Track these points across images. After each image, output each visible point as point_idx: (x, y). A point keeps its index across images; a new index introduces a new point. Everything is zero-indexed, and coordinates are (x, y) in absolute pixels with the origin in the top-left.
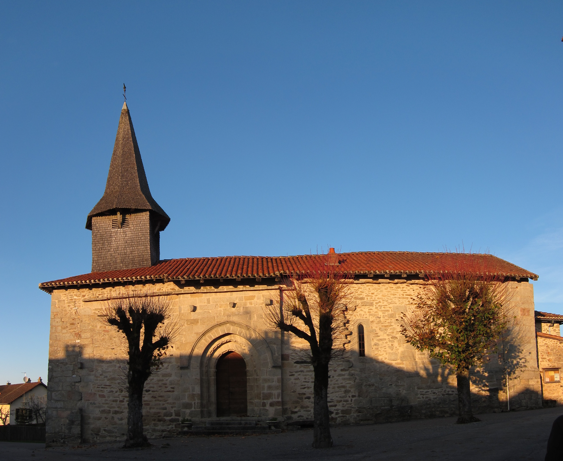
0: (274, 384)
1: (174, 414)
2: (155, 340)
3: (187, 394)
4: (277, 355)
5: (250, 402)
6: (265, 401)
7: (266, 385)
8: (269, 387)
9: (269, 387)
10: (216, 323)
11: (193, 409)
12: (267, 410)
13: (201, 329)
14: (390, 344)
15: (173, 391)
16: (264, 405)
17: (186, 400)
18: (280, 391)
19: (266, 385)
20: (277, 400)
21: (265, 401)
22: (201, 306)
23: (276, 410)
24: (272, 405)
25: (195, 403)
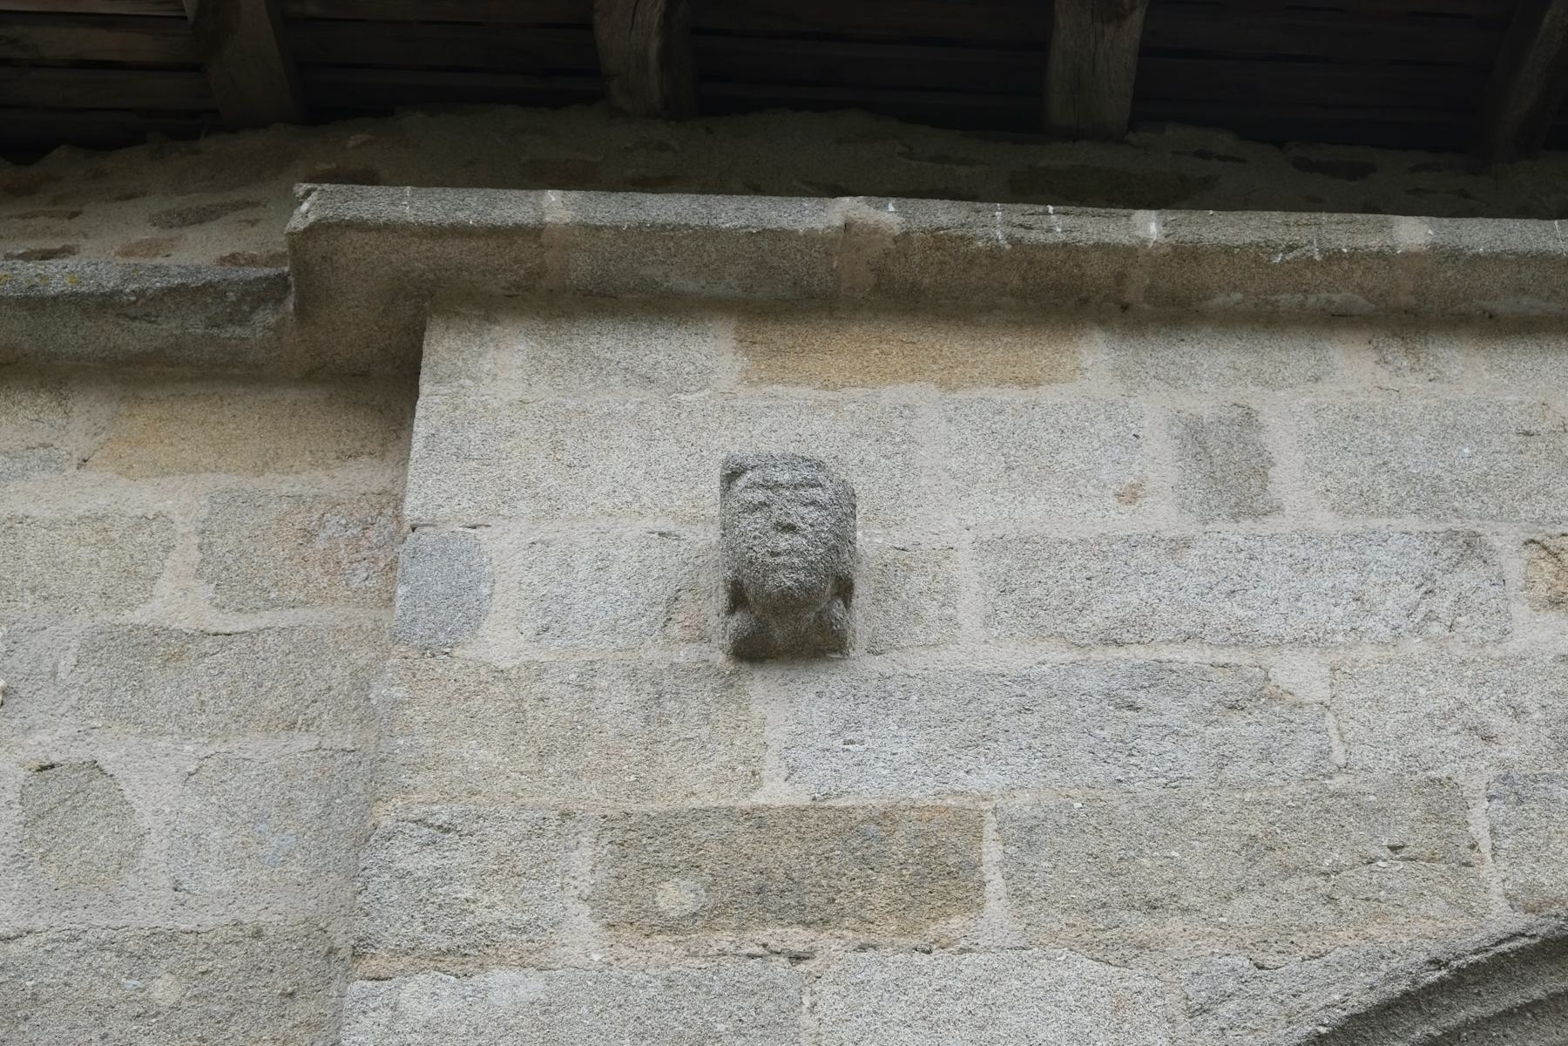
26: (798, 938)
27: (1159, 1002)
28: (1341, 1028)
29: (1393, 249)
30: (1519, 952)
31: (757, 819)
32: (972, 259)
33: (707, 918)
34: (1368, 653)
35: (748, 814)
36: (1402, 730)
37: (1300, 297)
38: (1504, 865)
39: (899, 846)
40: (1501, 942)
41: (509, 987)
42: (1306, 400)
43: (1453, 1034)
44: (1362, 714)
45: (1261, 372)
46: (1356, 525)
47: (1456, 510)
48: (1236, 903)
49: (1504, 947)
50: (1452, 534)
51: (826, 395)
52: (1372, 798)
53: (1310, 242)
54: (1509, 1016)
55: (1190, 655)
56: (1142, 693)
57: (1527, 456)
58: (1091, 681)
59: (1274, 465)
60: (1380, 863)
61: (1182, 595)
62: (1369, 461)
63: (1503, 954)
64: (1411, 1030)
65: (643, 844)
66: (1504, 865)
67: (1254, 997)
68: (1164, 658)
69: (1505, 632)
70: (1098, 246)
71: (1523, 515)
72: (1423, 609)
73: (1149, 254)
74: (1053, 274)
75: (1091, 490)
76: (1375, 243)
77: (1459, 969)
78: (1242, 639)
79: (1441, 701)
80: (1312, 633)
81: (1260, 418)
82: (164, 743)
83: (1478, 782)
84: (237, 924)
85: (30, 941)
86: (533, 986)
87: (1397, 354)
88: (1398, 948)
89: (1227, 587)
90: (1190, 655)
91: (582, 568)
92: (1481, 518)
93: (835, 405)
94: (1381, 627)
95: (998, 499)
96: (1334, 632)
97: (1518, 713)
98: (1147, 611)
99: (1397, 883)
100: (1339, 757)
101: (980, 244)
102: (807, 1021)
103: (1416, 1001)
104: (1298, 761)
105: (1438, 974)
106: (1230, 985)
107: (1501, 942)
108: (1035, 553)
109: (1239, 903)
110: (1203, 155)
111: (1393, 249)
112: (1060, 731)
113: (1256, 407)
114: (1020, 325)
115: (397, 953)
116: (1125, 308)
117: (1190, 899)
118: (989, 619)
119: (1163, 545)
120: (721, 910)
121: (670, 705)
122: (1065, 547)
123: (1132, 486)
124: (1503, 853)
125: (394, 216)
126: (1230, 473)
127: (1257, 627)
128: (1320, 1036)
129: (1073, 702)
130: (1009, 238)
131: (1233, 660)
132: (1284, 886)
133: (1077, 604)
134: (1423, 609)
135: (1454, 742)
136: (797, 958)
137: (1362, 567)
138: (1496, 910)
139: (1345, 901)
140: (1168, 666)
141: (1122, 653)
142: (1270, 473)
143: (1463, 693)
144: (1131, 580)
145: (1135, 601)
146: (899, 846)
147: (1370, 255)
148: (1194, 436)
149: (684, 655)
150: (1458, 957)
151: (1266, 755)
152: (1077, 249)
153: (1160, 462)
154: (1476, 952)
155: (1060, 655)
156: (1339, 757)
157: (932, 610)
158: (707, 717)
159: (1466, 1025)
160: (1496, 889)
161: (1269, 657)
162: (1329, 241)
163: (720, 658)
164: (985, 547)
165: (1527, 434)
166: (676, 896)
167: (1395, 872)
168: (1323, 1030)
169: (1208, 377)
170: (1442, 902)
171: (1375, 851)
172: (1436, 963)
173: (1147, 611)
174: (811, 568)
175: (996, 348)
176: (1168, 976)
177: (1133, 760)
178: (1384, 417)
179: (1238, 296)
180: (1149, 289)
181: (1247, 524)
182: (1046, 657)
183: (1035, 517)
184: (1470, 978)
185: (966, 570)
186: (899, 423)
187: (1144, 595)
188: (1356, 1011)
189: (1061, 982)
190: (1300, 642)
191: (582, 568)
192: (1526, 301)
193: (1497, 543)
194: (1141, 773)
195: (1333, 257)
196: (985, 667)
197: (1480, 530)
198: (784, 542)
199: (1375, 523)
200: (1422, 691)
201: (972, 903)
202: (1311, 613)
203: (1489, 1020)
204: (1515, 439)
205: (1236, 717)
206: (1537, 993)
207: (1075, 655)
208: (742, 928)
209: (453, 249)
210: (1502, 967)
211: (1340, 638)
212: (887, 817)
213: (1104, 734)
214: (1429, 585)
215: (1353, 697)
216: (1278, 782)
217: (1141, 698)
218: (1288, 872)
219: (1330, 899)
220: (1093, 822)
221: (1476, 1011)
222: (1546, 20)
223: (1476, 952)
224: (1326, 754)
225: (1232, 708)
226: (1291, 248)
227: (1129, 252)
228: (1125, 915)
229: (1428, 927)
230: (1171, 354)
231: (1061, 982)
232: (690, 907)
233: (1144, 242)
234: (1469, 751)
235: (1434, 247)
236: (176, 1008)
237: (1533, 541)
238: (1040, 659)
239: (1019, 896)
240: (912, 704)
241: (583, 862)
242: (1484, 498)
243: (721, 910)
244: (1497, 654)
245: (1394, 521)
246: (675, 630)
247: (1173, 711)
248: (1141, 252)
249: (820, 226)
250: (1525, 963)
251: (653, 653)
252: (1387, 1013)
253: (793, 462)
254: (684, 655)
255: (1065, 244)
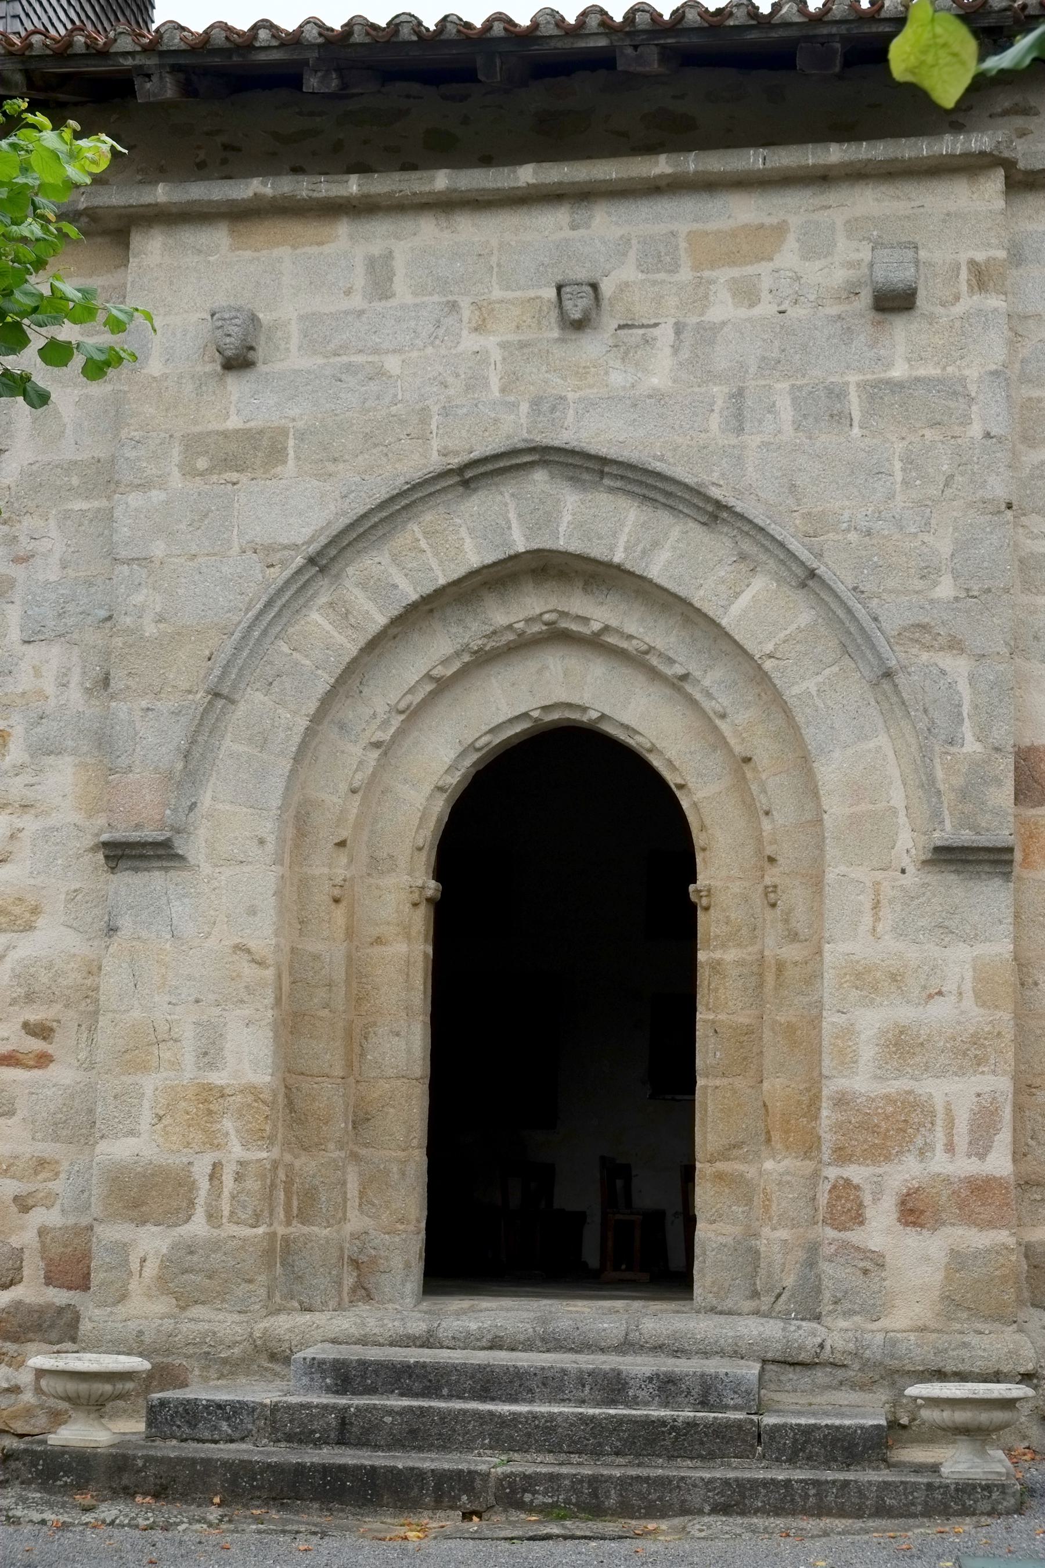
0: (940, 1012)
1: (33, 1268)
2: (754, 22)
3: (149, 1083)
4: (971, 746)
5: (720, 1176)
6: (855, 1173)
7: (871, 1022)
8: (901, 1046)
9: (901, 1046)
10: (435, 462)
11: (198, 1227)
12: (874, 1263)
13: (300, 509)
14: (877, 1377)
15: (43, 1060)
16: (847, 1208)
17: (134, 1146)
18: (1004, 1084)
19: (871, 1022)
20: (966, 1166)
21: (855, 1173)
22: (311, 320)
23: (958, 1260)
24: (913, 1212)
25: (215, 1175)
26: (234, 476)
31: (225, 434)
33: (209, 471)
35: (223, 433)
39: (265, 442)
41: (157, 496)
46: (418, 300)
50: (448, 302)
51: (256, 254)
55: (359, 359)
62: (426, 271)
65: (193, 444)
78: (376, 351)
82: (69, 390)
84: (93, 457)
85: (37, 465)
86: (163, 496)
89: (374, 330)
90: (359, 359)
91: (179, 335)
93: (258, 259)
100: (400, 397)
102: (236, 505)
106: (353, 488)
115: (127, 486)
117: (347, 457)
118: (300, 348)
120: (214, 467)
121: (204, 388)
125: (110, 204)
136: (234, 484)
139: (390, 455)
146: (265, 442)
148: (371, 263)
149: (208, 368)
155: (320, 361)
156: (400, 397)
157: (283, 346)
158: (214, 392)
163: (219, 368)
164: (301, 318)
166: (202, 463)
169: (378, 237)
171: (402, 436)
172: (407, 483)
174: (237, 348)
181: (384, 302)
185: (294, 329)
186: (278, 265)
189: (306, 489)
190: (394, 351)
191: (179, 335)
196: (296, 367)
198: (228, 340)
201: (285, 462)
205: (371, 384)
206: (438, 487)
208: (220, 474)
209: (132, 210)
212: (261, 432)
217: (343, 377)
218: (376, 445)
221: (421, 494)
224: (396, 396)
229: (412, 463)
231: (306, 489)
232: (206, 467)
236: (79, 486)
239: (298, 458)
240: (274, 384)
241: (176, 453)
243: (214, 467)
246: (206, 358)
249: (245, 197)
251: (199, 368)
253: (230, 308)
254: (208, 368)
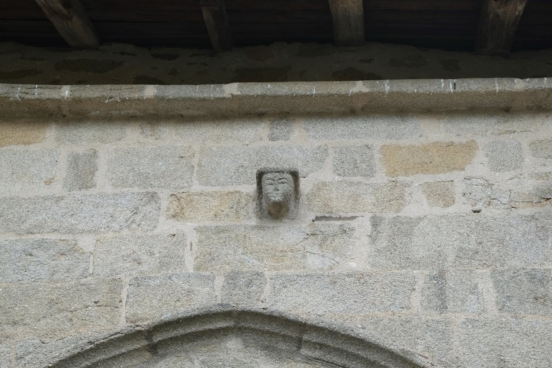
27: (8, 355)
28: (57, 364)
29: (143, 97)
30: (118, 339)
32: (11, 103)
34: (110, 235)
36: (113, 261)
37: (118, 112)
38: (128, 307)
40: (112, 335)
42: (114, 147)
43: (95, 364)
44: (103, 256)
45: (103, 137)
46: (117, 191)
47: (151, 185)
48: (41, 322)
49: (112, 337)
52: (93, 286)
53: (117, 96)
54: (114, 358)
55: (53, 237)
56: (35, 250)
57: (179, 165)
58: (20, 246)
59: (97, 170)
60: (90, 308)
61: (56, 216)
62: (128, 168)
63: (112, 339)
64: (81, 364)
66: (128, 307)
67: (38, 353)
68: (45, 238)
69: (155, 227)
70: (48, 99)
71: (172, 185)
72: (131, 219)
73: (65, 101)
74: (38, 107)
75: (37, 180)
76: (136, 96)
77: (97, 344)
79: (128, 251)
80: (94, 229)
81: (98, 154)
83: (128, 280)
87: (148, 130)
88: (86, 336)
90: (53, 237)
92: (159, 187)
94: (116, 226)
95: (7, 184)
96: (101, 228)
97: (152, 254)
98: (43, 222)
99: (93, 314)
101: (12, 99)
103: (83, 355)
104: (78, 272)
105: (90, 346)
106: (31, 349)
107: (112, 335)
108: (13, 203)
109: (43, 322)
110: (122, 53)
111: (143, 97)
112: (6, 264)
113: (97, 150)
114: (29, 123)
116: (64, 116)
119: (55, 199)
122: (23, 201)
123: (51, 179)
124: (129, 303)
126: (82, 173)
127: (77, 226)
128: (49, 367)
129: (12, 254)
130: (20, 97)
131: (67, 238)
132: (58, 316)
133: (22, 220)
134: (131, 219)
135: (128, 265)
137: (115, 205)
138: (121, 322)
139: (75, 320)
140: (45, 241)
141: (33, 236)
142: (96, 173)
143: (136, 248)
144: (41, 212)
145: (40, 218)
147: (135, 99)
148: (75, 160)
150: (97, 341)
151: (68, 271)
152: (42, 100)
153: (62, 171)
154: (103, 339)
159: (100, 361)
160: (124, 315)
161: (78, 237)
162: (122, 95)
165: (182, 157)
167: (94, 310)
168: (50, 365)
169: (85, 139)
170: (105, 320)
172: (90, 343)
173: (43, 222)
175: (20, 131)
176: (12, 347)
177: (26, 273)
178: (137, 153)
179: (98, 112)
180: (69, 111)
181: (83, 191)
182: (8, 238)
183: (17, 190)
184: (101, 347)
187: (44, 216)
188: (62, 359)
190: (89, 232)
192: (191, 111)
193: (161, 196)
194: (27, 277)
195: (124, 100)
197: (157, 191)
199: (125, 190)
200: (123, 248)
202: (95, 222)
203: (108, 359)
204: (177, 159)
205: (63, 258)
206: (123, 350)
207: (18, 238)
210: (112, 343)
211: (102, 230)
213: (19, 264)
214: (136, 211)
215: (101, 250)
216: (69, 279)
217: (34, 252)
218: (60, 311)
219: (71, 320)
220: (4, 295)
221: (104, 357)
222: (205, 17)
223: (103, 339)
224: (87, 270)
225: (62, 254)
226: (111, 98)
227: (59, 101)
228: (5, 326)
229: (98, 328)
230: (75, 132)
233: (63, 97)
234: (132, 268)
235: (156, 96)
237: (173, 195)
238: (6, 239)
242: (162, 180)
244: (150, 234)
245: (130, 189)
247: (42, 255)
248: (63, 100)
250: (120, 341)
252: (73, 359)
255: (38, 99)
